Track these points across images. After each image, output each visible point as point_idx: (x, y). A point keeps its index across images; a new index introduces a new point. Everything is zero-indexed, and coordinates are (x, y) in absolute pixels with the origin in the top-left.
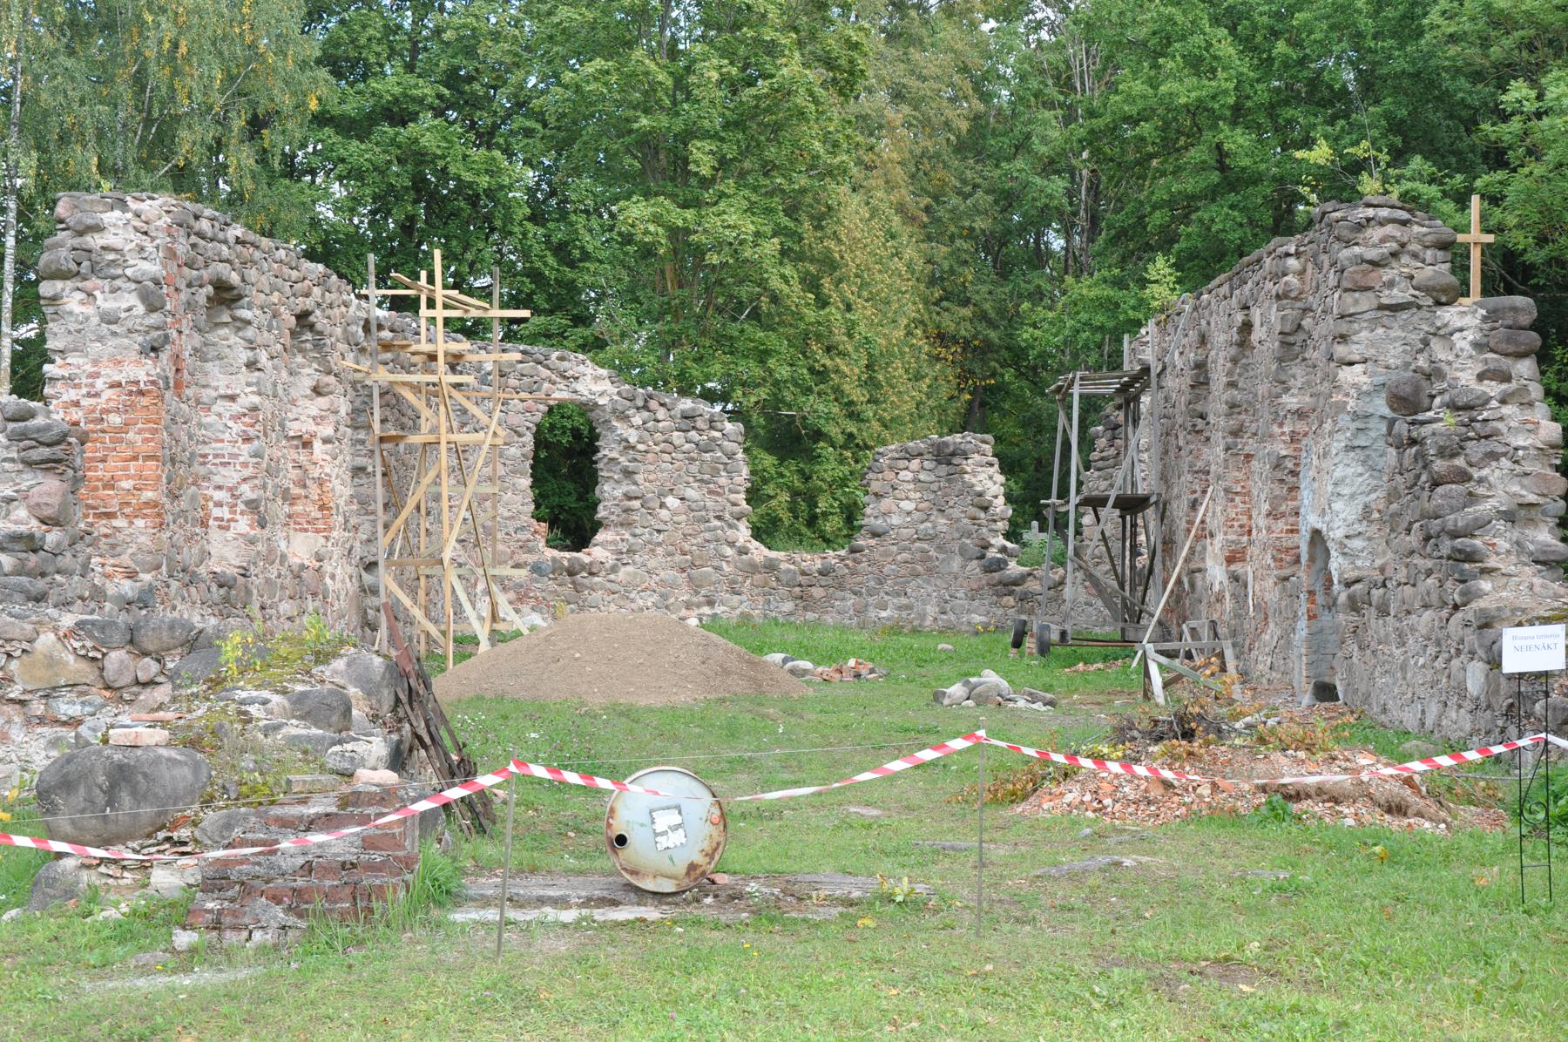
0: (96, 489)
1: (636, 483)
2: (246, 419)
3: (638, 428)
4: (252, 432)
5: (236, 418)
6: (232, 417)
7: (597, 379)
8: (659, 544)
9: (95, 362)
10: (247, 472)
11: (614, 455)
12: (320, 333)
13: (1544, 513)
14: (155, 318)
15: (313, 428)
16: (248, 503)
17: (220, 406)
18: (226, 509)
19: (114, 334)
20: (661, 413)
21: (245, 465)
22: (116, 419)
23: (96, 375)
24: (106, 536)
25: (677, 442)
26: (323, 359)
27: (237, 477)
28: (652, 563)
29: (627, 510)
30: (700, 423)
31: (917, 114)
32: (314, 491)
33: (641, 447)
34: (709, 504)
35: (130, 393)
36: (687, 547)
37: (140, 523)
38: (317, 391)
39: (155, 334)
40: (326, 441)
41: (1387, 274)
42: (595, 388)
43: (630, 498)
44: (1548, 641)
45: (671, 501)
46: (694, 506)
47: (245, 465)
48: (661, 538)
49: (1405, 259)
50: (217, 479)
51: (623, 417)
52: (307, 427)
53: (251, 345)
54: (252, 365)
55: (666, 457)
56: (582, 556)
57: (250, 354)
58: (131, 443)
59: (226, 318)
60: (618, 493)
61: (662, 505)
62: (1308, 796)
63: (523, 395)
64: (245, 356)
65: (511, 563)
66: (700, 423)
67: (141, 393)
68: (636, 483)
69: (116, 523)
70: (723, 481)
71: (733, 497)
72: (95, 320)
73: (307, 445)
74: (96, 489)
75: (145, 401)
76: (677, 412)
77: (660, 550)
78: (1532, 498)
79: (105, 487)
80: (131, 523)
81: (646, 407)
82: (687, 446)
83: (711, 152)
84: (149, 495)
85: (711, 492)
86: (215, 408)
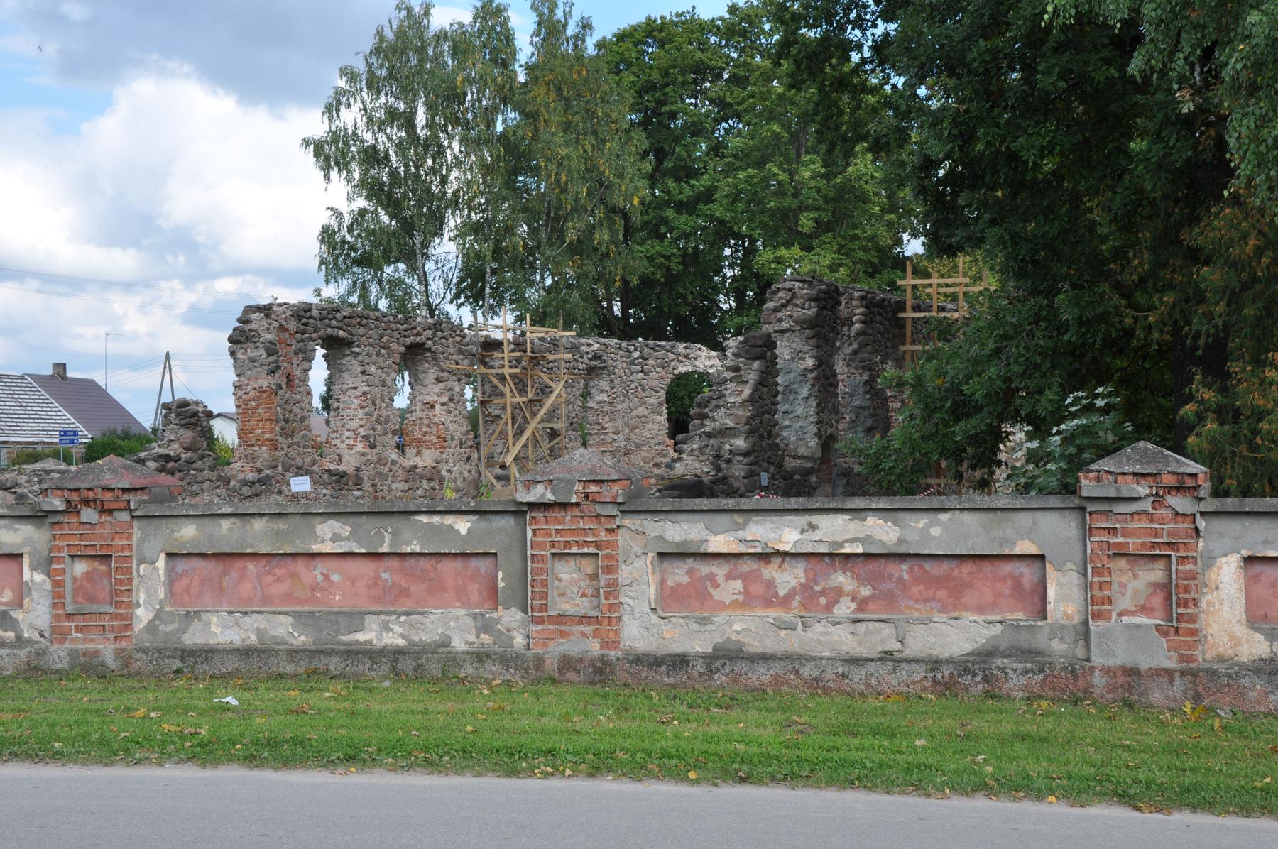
4: (364, 404)
5: (356, 398)
7: (709, 358)
10: (362, 423)
14: (272, 359)
17: (350, 392)
22: (253, 404)
26: (438, 365)
32: (434, 429)
37: (264, 448)
38: (438, 380)
40: (443, 404)
41: (780, 315)
49: (789, 308)
50: (347, 426)
54: (363, 373)
64: (360, 369)
73: (433, 407)
78: (732, 425)
84: (267, 436)
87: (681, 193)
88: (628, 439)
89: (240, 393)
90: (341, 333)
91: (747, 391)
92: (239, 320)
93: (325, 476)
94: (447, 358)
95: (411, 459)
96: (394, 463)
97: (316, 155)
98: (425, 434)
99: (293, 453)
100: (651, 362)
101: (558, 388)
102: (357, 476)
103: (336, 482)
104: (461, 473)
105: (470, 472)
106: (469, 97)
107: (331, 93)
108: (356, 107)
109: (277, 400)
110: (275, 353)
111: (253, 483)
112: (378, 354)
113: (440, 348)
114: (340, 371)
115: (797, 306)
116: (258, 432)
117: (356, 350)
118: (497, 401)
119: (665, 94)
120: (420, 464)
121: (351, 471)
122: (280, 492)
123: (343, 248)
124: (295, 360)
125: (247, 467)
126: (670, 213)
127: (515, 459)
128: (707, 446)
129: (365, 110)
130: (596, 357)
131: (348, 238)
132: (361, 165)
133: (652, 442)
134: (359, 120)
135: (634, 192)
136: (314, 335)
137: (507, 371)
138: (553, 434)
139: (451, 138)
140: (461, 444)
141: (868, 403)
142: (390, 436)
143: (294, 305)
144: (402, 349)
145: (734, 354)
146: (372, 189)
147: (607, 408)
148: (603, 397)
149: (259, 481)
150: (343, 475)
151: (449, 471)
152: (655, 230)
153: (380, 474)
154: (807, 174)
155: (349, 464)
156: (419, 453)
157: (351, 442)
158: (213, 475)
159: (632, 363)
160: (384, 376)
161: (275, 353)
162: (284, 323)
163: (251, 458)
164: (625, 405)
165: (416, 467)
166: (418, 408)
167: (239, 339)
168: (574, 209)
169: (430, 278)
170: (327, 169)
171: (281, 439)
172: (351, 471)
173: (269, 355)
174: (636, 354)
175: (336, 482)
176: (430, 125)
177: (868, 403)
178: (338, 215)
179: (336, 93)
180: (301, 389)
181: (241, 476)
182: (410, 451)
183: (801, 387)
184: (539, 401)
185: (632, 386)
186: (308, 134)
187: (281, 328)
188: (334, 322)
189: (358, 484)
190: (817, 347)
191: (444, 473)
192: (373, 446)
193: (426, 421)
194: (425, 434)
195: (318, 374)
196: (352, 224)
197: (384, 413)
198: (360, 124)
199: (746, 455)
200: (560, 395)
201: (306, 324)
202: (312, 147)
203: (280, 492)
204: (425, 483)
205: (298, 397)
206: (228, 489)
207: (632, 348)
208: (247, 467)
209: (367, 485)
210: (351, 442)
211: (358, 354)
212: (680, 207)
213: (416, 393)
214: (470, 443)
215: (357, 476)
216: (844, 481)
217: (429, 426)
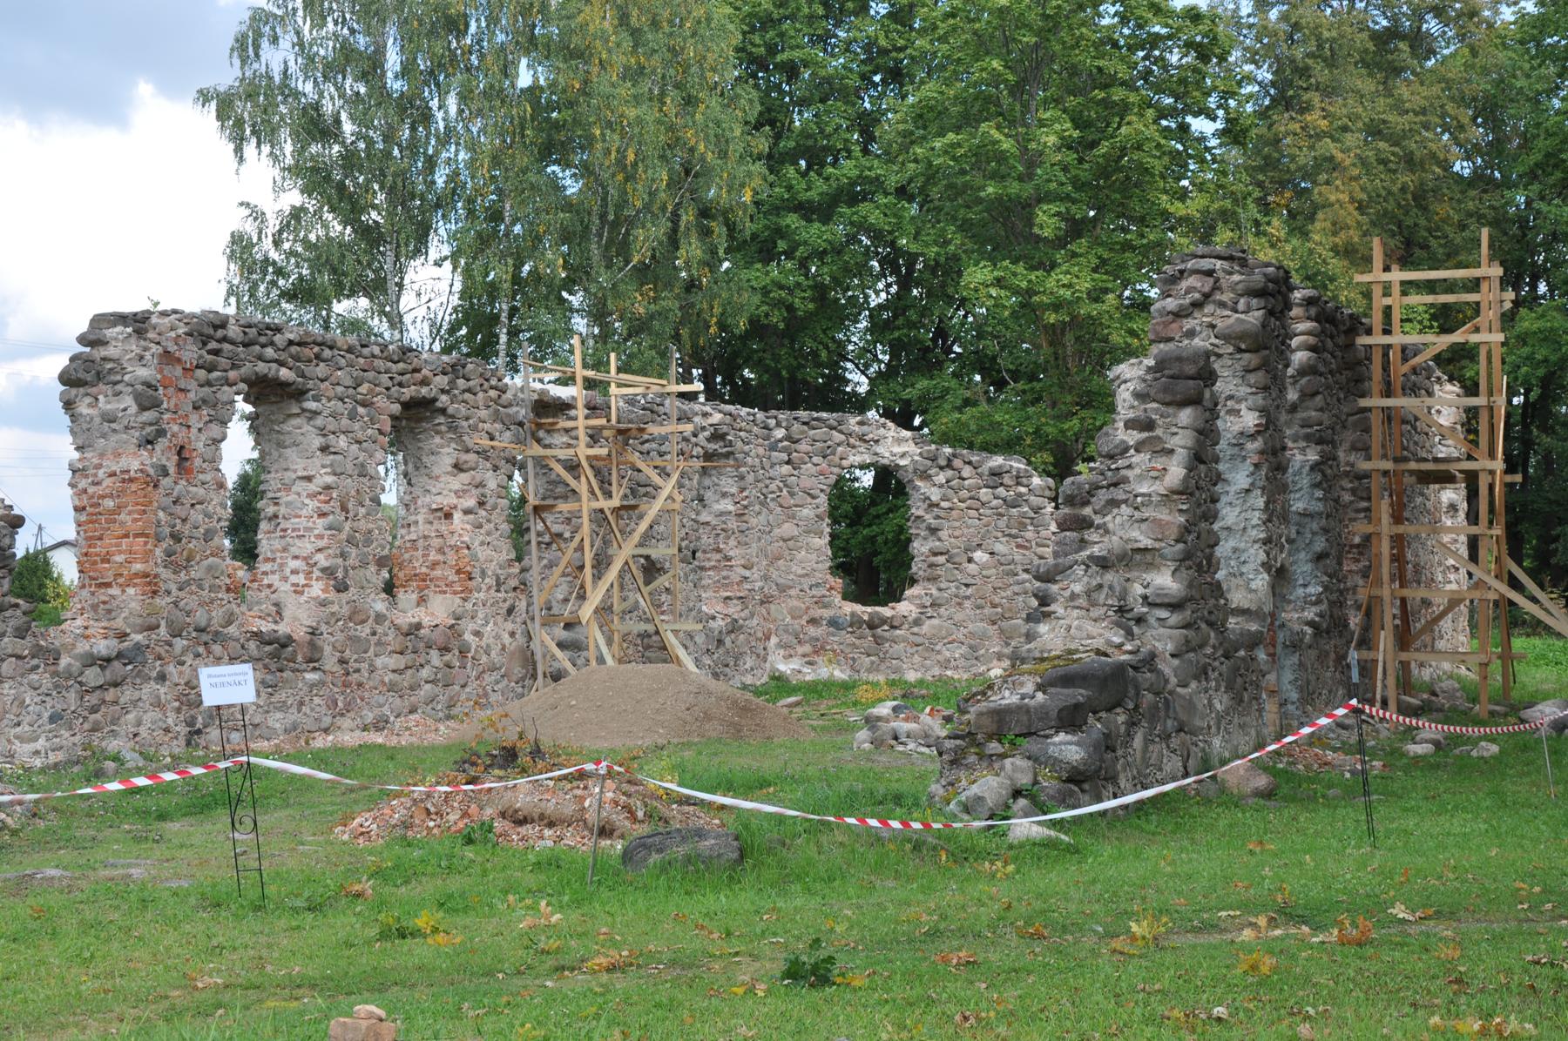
0: (95, 563)
1: (939, 540)
2: (322, 497)
3: (941, 486)
4: (326, 508)
5: (312, 496)
6: (309, 496)
7: (899, 441)
8: (968, 598)
9: (102, 456)
10: (321, 544)
11: (920, 513)
12: (452, 416)
13: (1163, 557)
14: (149, 416)
15: (455, 501)
16: (323, 570)
17: (300, 486)
18: (302, 576)
19: (114, 431)
20: (967, 471)
21: (320, 537)
22: (109, 503)
23: (99, 466)
24: (104, 603)
25: (984, 499)
27: (310, 548)
28: (959, 616)
29: (931, 566)
30: (1007, 480)
31: (1397, 149)
32: (451, 557)
33: (944, 504)
34: (1018, 558)
35: (124, 481)
36: (997, 600)
37: (131, 591)
38: (458, 467)
39: (149, 429)
40: (467, 512)
41: (1189, 324)
42: (896, 449)
43: (936, 554)
44: (238, 678)
45: (979, 555)
46: (1002, 560)
47: (320, 537)
48: (969, 591)
49: (1209, 309)
51: (925, 476)
52: (448, 500)
53: (322, 431)
54: (324, 449)
55: (973, 513)
56: (886, 611)
57: (322, 440)
58: (122, 523)
59: (296, 410)
60: (925, 549)
61: (970, 560)
62: (533, 821)
63: (815, 460)
64: (318, 442)
65: (806, 618)
66: (1007, 480)
67: (131, 480)
68: (939, 540)
69: (112, 591)
70: (1030, 535)
71: (1040, 550)
72: (97, 420)
73: (448, 516)
74: (95, 563)
75: (134, 487)
76: (985, 469)
77: (967, 604)
78: (1146, 542)
79: (103, 561)
80: (124, 591)
81: (949, 465)
82: (995, 502)
83: (1058, 214)
84: (138, 567)
85: (1018, 546)
86: (294, 488)
87: (809, 189)
88: (766, 578)
89: (83, 484)
90: (284, 374)
91: (1176, 472)
92: (82, 340)
93: (252, 645)
94: (474, 428)
95: (408, 611)
96: (380, 618)
97: (220, 116)
98: (434, 565)
99: (190, 601)
100: (803, 447)
101: (668, 486)
102: (312, 644)
103: (273, 655)
104: (497, 637)
105: (512, 634)
106: (473, 28)
107: (246, 16)
108: (287, 41)
109: (158, 496)
110: (155, 405)
111: (108, 660)
112: (353, 416)
113: (463, 410)
114: (281, 445)
115: (1222, 305)
116: (119, 558)
117: (312, 405)
118: (563, 507)
119: (782, 35)
120: (426, 621)
121: (300, 634)
122: (162, 678)
123: (265, 273)
124: (194, 420)
125: (96, 628)
126: (792, 220)
127: (596, 611)
128: (1100, 586)
129: (301, 44)
130: (717, 436)
131: (274, 255)
132: (295, 135)
133: (806, 583)
134: (291, 64)
135: (741, 185)
136: (232, 374)
137: (583, 451)
138: (652, 569)
139: (443, 93)
140: (499, 584)
141: (1320, 507)
142: (373, 568)
143: (193, 316)
144: (396, 408)
145: (1138, 395)
146: (313, 178)
147: (733, 524)
148: (727, 505)
149: (119, 655)
150: (285, 642)
151: (477, 634)
152: (764, 249)
153: (354, 640)
154: (1052, 140)
155: (296, 620)
156: (422, 601)
157: (301, 579)
158: (24, 647)
159: (773, 448)
160: (362, 456)
161: (155, 405)
162: (172, 348)
163: (105, 610)
164: (762, 518)
165: (418, 626)
166: (420, 518)
167: (83, 376)
168: (647, 207)
169: (407, 319)
170: (239, 142)
171: (165, 573)
172: (300, 634)
173: (143, 408)
174: (780, 433)
175: (273, 655)
176: (406, 71)
177: (1320, 507)
178: (258, 216)
179: (253, 19)
180: (207, 477)
181: (83, 647)
182: (406, 597)
183: (1233, 469)
184: (634, 507)
185: (773, 487)
186: (206, 84)
187: (167, 357)
188: (269, 352)
189: (313, 660)
190: (1266, 388)
191: (468, 637)
192: (341, 588)
193: (436, 542)
194: (434, 565)
195: (237, 449)
196: (280, 232)
197: (362, 525)
198: (293, 68)
199: (1175, 606)
200: (670, 497)
201: (216, 352)
202: (213, 105)
203: (162, 678)
204: (434, 654)
205: (201, 491)
206: (55, 674)
207: (772, 422)
208: (96, 628)
209: (330, 661)
210: (301, 579)
211: (316, 413)
212: (807, 210)
213: (417, 491)
214: (514, 583)
215: (312, 644)
216: (1295, 659)
217: (441, 551)
